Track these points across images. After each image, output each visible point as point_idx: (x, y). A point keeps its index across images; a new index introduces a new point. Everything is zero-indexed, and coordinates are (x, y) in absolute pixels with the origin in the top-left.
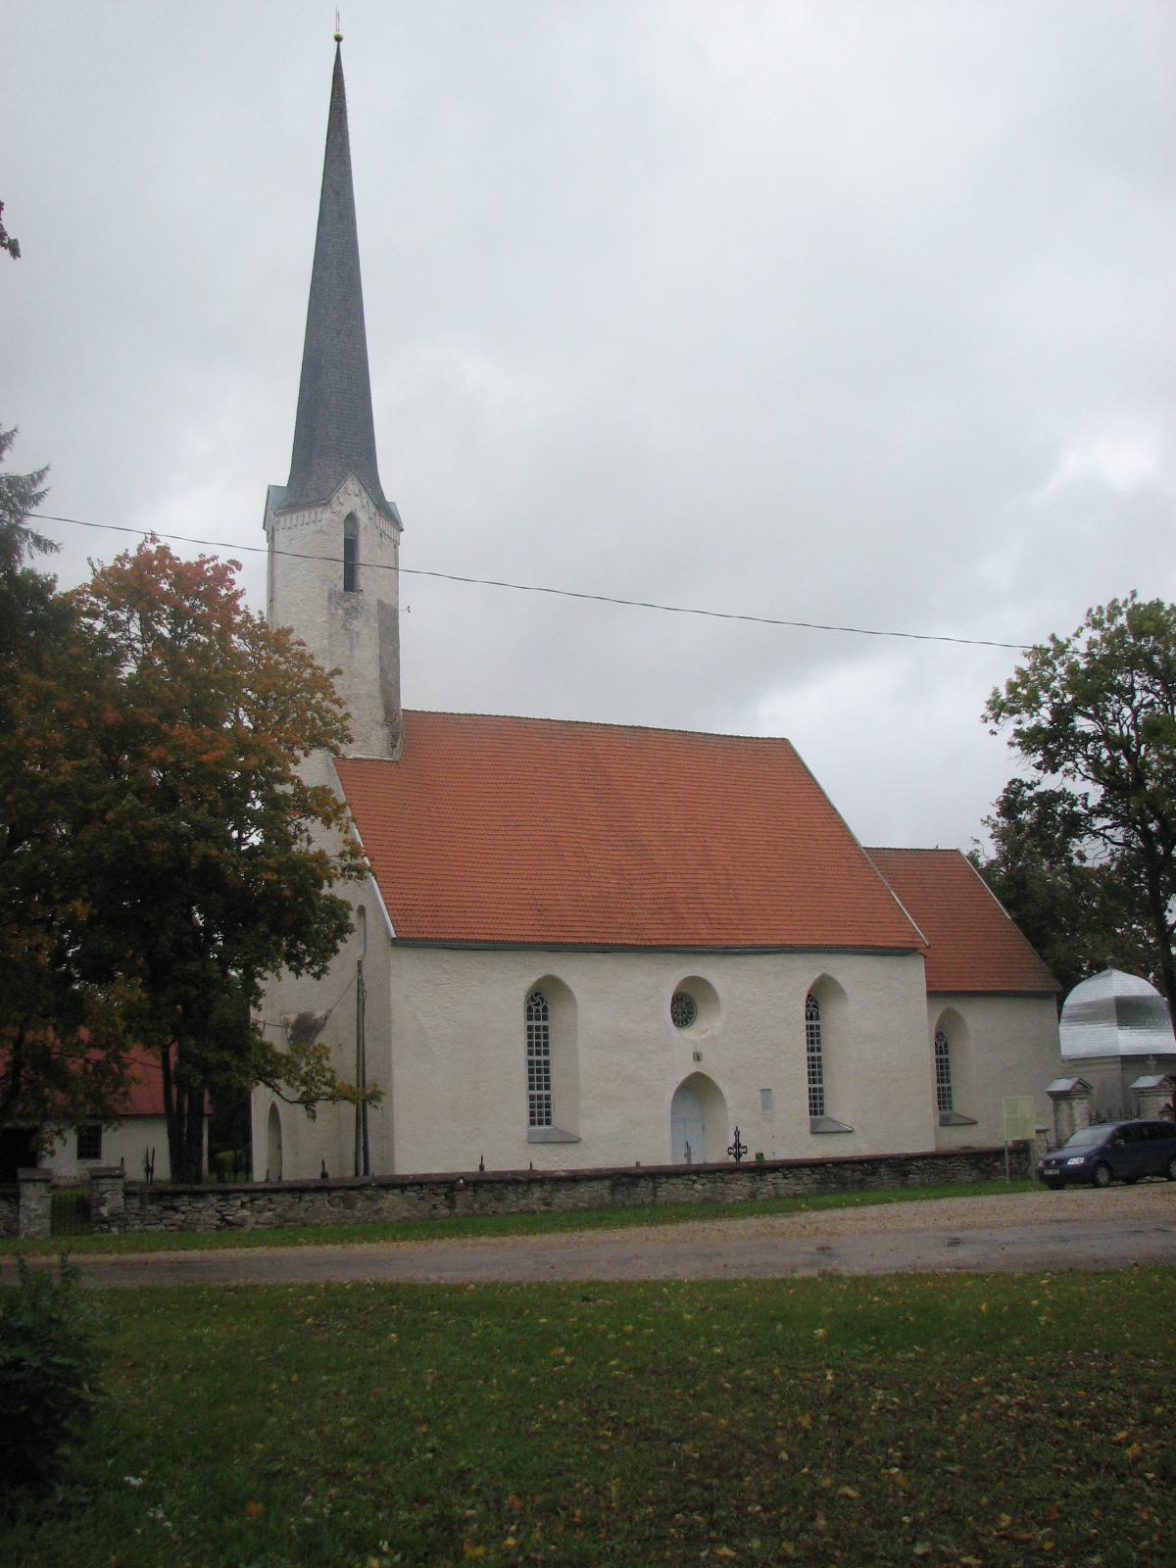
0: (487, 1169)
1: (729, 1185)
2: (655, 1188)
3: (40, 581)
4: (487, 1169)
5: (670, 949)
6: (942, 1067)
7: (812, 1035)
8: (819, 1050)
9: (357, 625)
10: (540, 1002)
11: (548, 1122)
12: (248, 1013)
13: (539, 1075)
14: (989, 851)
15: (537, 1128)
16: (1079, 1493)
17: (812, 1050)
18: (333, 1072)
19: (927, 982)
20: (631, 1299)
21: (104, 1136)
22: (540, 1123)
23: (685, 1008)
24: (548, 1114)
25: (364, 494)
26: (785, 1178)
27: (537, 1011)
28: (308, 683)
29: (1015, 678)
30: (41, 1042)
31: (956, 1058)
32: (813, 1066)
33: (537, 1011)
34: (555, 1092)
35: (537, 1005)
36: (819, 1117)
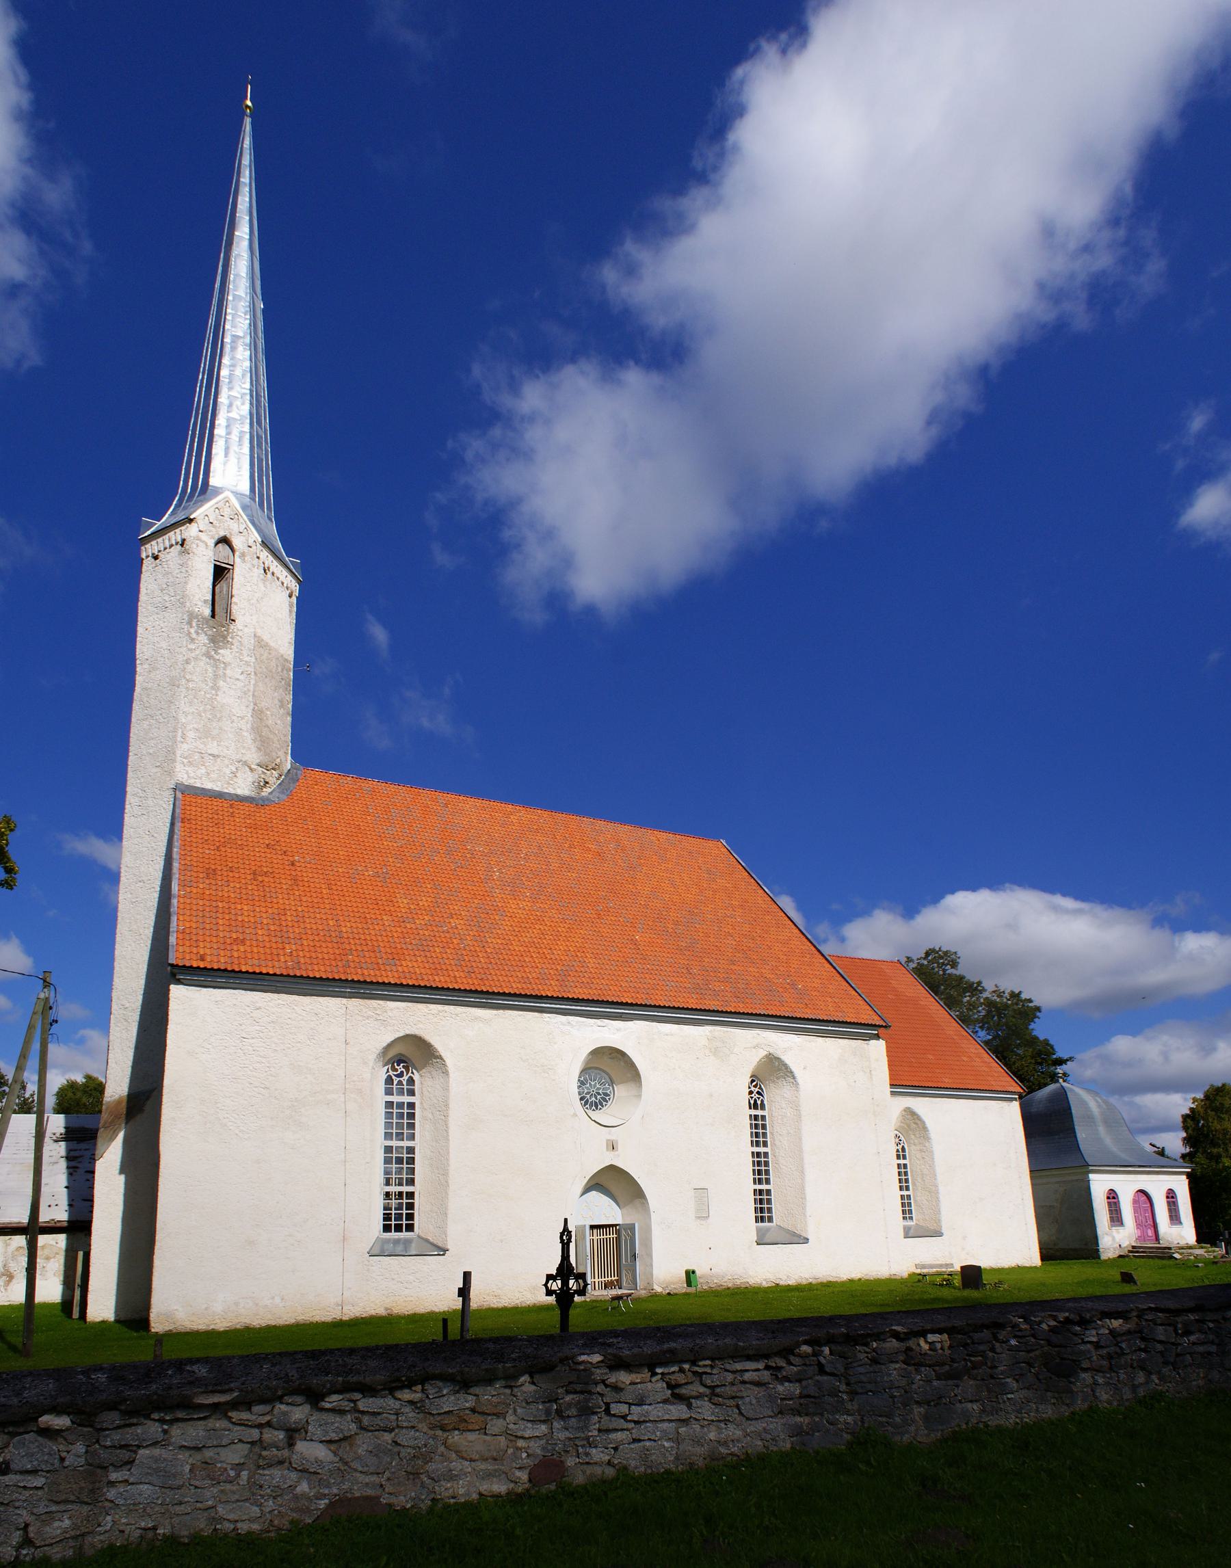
0: (477, 1299)
1: (456, 1438)
2: (96, 1469)
3: (739, 94)
4: (477, 1299)
5: (649, 1348)
6: (762, 1210)
7: (756, 1126)
8: (768, 1182)
9: (225, 654)
10: (409, 1057)
11: (410, 1228)
12: (29, 949)
14: (1091, 1176)
15: (394, 1235)
16: (260, 684)
17: (755, 1107)
18: (549, 1277)
19: (93, 1172)
20: (233, 226)
21: (1194, 1238)
22: (398, 1228)
23: (608, 1072)
24: (410, 1217)
25: (610, 1472)
26: (677, 1395)
27: (400, 1083)
28: (677, 1391)
29: (1023, 996)
30: (609, 1463)
31: (778, 1149)
32: (761, 1201)
33: (400, 1083)
34: (422, 1143)
35: (401, 1075)
36: (766, 1224)
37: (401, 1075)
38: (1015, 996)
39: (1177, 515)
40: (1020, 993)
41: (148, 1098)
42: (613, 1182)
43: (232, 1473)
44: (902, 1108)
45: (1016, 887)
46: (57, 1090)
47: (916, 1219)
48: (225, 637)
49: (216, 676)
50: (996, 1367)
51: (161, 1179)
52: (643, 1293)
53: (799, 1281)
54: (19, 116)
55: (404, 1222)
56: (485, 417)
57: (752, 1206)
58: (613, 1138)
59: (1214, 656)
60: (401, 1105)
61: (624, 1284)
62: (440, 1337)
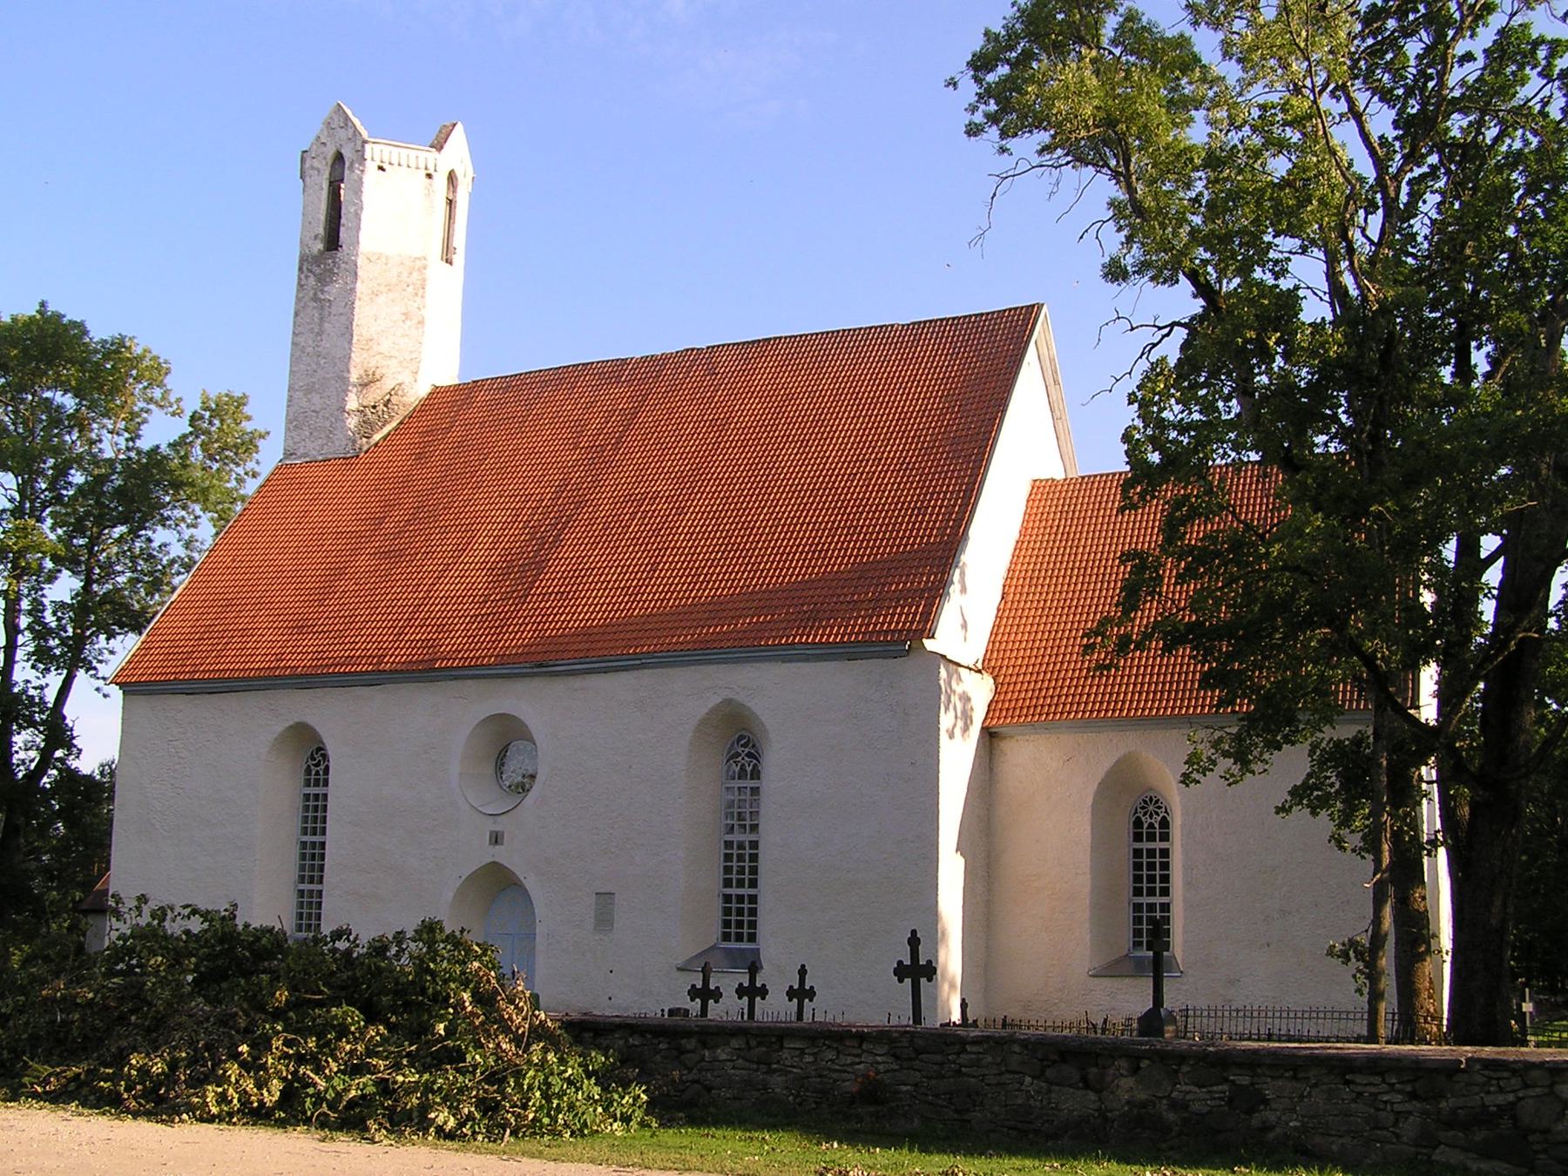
13: (314, 813)
15: (733, 945)
37: (317, 765)
38: (169, 1122)
39: (1442, 665)
40: (987, 33)
41: (1118, 961)
42: (497, 884)
43: (49, 564)
44: (280, 727)
45: (939, 1002)
46: (71, 315)
47: (740, 747)
48: (159, 368)
49: (322, 319)
50: (130, 580)
51: (1014, 535)
52: (776, 1008)
53: (1014, 1013)
54: (80, 327)
55: (1158, 860)
56: (1335, 1166)
57: (1007, 564)
58: (498, 828)
59: (1504, 471)
60: (740, 899)
61: (1382, 1032)
62: (904, 1017)
